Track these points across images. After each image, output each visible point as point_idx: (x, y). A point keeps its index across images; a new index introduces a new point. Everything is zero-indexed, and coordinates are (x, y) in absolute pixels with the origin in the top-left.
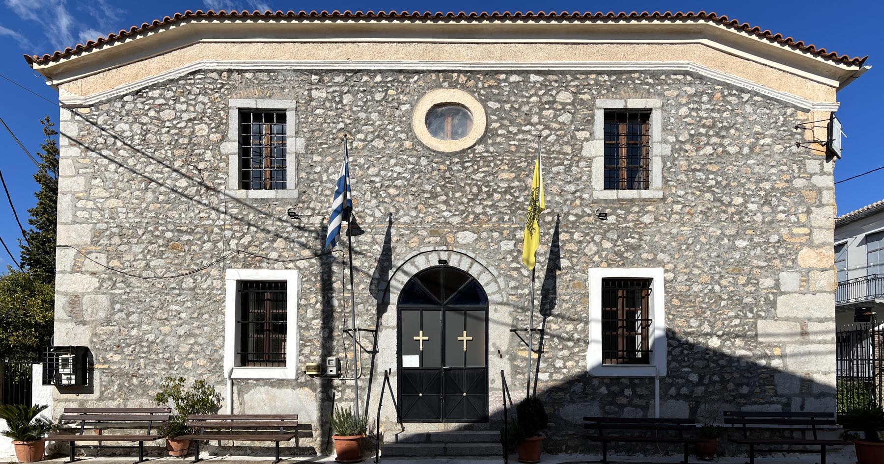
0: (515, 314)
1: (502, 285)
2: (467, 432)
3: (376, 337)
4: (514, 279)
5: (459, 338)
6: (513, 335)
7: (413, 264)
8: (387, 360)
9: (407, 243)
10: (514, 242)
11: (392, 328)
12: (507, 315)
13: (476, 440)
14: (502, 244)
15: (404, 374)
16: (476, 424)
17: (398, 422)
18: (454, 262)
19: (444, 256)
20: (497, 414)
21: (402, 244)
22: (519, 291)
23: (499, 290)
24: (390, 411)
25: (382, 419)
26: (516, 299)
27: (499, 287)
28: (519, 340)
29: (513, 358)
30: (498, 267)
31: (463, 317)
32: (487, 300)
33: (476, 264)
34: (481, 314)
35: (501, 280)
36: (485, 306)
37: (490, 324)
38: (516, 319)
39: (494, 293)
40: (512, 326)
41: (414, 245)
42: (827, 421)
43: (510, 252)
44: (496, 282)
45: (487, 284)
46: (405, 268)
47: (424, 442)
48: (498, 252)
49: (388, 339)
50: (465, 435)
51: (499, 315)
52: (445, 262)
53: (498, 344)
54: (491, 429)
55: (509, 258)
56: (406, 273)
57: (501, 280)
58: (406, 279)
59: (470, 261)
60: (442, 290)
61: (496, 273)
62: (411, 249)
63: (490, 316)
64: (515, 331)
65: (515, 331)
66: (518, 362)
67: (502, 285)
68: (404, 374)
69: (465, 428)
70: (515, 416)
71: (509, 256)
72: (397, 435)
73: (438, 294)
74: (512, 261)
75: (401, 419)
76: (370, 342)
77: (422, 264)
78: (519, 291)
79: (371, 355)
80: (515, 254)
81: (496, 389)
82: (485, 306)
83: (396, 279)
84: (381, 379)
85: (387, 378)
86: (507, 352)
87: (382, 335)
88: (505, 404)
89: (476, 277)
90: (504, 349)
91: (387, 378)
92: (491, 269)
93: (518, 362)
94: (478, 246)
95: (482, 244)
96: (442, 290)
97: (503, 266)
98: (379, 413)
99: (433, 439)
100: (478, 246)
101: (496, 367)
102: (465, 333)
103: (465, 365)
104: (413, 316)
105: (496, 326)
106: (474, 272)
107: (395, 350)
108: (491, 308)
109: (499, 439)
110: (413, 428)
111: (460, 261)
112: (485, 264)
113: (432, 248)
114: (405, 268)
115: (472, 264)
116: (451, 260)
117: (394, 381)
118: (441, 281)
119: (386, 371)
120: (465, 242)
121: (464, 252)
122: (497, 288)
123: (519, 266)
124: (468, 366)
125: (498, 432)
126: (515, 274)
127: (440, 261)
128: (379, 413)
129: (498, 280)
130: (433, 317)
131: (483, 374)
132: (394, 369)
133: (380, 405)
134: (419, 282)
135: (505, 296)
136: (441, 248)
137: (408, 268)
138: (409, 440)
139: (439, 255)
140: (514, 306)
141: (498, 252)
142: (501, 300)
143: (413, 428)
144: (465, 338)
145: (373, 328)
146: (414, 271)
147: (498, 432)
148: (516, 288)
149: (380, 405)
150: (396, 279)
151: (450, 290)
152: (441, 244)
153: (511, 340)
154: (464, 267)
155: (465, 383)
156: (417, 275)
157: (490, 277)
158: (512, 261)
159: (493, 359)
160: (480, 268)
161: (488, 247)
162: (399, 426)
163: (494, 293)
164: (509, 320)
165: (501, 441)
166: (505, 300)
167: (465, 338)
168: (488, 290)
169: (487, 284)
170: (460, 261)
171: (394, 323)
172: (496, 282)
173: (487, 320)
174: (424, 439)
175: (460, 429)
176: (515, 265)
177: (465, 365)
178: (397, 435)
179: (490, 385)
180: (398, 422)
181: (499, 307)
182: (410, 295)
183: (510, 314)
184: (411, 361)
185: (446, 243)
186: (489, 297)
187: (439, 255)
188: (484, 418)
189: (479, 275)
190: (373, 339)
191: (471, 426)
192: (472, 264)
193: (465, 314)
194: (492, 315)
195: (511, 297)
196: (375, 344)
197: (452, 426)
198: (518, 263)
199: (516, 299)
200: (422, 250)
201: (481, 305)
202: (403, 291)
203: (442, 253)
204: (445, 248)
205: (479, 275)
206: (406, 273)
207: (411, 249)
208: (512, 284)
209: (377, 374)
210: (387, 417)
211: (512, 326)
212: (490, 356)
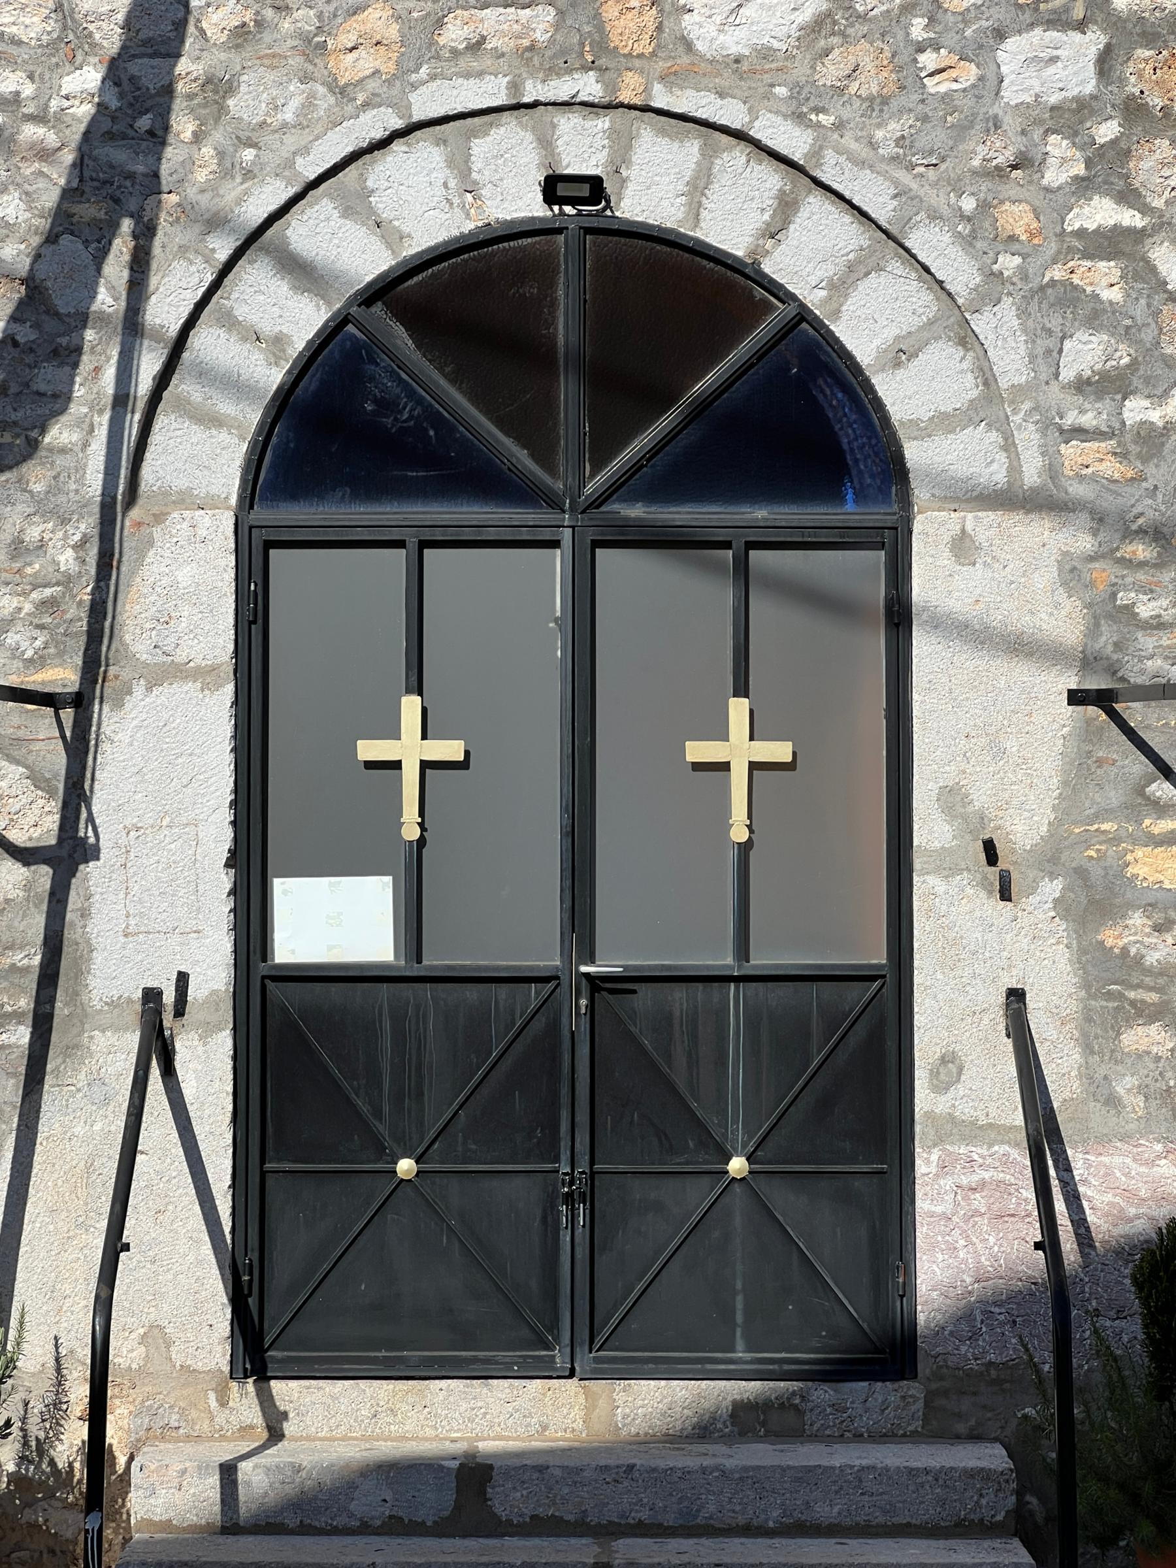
0: (1104, 572)
1: (1011, 363)
2: (758, 1454)
3: (80, 748)
4: (1096, 315)
5: (698, 751)
6: (1088, 734)
7: (357, 206)
8: (155, 911)
9: (313, 47)
10: (1093, 41)
11: (204, 675)
12: (1045, 577)
13: (826, 1511)
14: (1012, 54)
15: (294, 1032)
16: (823, 1394)
17: (238, 1372)
18: (651, 194)
19: (582, 149)
20: (987, 1312)
21: (273, 61)
22: (1136, 410)
23: (989, 403)
24: (181, 1293)
25: (122, 1353)
26: (1111, 468)
27: (986, 377)
28: (1139, 765)
29: (1095, 900)
30: (978, 233)
31: (728, 596)
32: (893, 472)
33: (815, 205)
34: (861, 570)
35: (999, 326)
36: (877, 514)
37: (925, 650)
38: (1110, 612)
39: (946, 422)
40: (1088, 662)
41: (365, 62)
42: (688, 1358)
43: (1071, 117)
44: (967, 339)
45: (900, 355)
46: (306, 233)
47: (443, 1529)
48: (976, 113)
49: (169, 760)
50: (750, 1477)
51: (986, 576)
52: (595, 188)
53: (981, 797)
54: (937, 1427)
55: (1062, 162)
56: (302, 273)
57: (999, 326)
58: (303, 319)
59: (770, 180)
60: (568, 393)
61: (961, 274)
62: (342, 92)
63: (921, 589)
64: (1103, 699)
65: (1103, 699)
66: (1132, 932)
67: (1011, 363)
68: (294, 1032)
69: (745, 1421)
70: (1129, 1331)
71: (1058, 146)
72: (228, 1471)
73: (535, 430)
74: (1083, 187)
75: (258, 1349)
76: (37, 780)
77: (423, 207)
78: (1136, 410)
79: (44, 875)
80: (1107, 131)
81: (974, 1132)
82: (877, 514)
83: (229, 321)
84: (115, 1051)
85: (158, 1048)
86: (1050, 858)
87: (121, 730)
88: (1049, 1244)
89: (813, 298)
90: (1024, 829)
91: (158, 1048)
92: (927, 241)
93: (1132, 932)
94: (831, 72)
95: (863, 54)
96: (568, 393)
97: (1016, 217)
98: (104, 1305)
99: (507, 1501)
100: (831, 72)
101: (969, 963)
102: (738, 710)
103: (743, 950)
104: (341, 591)
105: (970, 663)
106: (806, 260)
107: (219, 835)
108: (931, 532)
109: (1000, 1505)
110: (348, 1421)
111: (698, 189)
112: (882, 208)
113: (493, 92)
114: (306, 233)
115: (786, 208)
116: (632, 173)
117: (207, 1065)
118: (564, 328)
119: (152, 996)
120: (735, 42)
121: (731, 114)
122: (966, 388)
123: (1131, 218)
124: (761, 960)
125: (992, 1457)
126: (1103, 280)
127: (554, 187)
128: (104, 1305)
129: (981, 324)
130: (503, 595)
131: (885, 997)
132: (213, 976)
133: (115, 1246)
134: (401, 337)
135: (1028, 438)
136: (562, 89)
137: (317, 232)
138: (318, 1512)
139: (546, 143)
140: (1099, 520)
141: (976, 113)
142: (996, 474)
143: (348, 1421)
144: (738, 744)
145: (63, 676)
146: (367, 261)
147: (992, 1457)
148: (1108, 385)
149: (115, 1246)
150: (229, 321)
151: (623, 392)
152: (559, 61)
153: (1081, 770)
154: (728, 228)
155: (737, 1075)
156: (381, 291)
157: (920, 303)
158: (1083, 187)
159: (945, 903)
160: (847, 235)
161: (907, 77)
162: (244, 1403)
163: (946, 422)
164: (1062, 620)
165: (1020, 1526)
166: (1032, 473)
167: (738, 744)
168: (902, 395)
169: (900, 355)
170: (698, 189)
171: (214, 637)
172: (967, 339)
173: (899, 617)
174: (437, 1501)
175: (704, 1431)
176: (1100, 213)
177: (743, 950)
178: (228, 1471)
179: (924, 1099)
180: (238, 1372)
181: (984, 524)
182: (338, 439)
183: (1072, 574)
184: (336, 920)
185: (598, 54)
186: (913, 453)
187: (546, 143)
188: (888, 1350)
189: (840, 287)
190: (59, 760)
191: (784, 1405)
192: (786, 208)
193: (742, 570)
194: (932, 579)
195: (1072, 451)
196: (75, 796)
197: (648, 1403)
198: (1129, 196)
199: (1111, 468)
200: (425, 106)
201: (851, 511)
202: (283, 404)
203: (568, 124)
204: (589, 87)
205: (840, 287)
206: (302, 273)
207: (342, 92)
208: (1085, 352)
209: (82, 1016)
210: (155, 1336)
211: (1088, 662)
212: (927, 888)
